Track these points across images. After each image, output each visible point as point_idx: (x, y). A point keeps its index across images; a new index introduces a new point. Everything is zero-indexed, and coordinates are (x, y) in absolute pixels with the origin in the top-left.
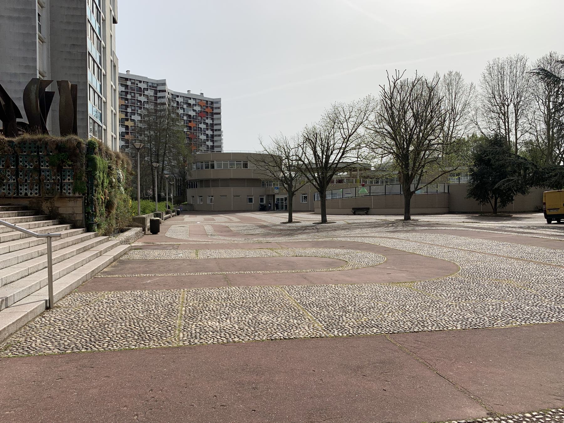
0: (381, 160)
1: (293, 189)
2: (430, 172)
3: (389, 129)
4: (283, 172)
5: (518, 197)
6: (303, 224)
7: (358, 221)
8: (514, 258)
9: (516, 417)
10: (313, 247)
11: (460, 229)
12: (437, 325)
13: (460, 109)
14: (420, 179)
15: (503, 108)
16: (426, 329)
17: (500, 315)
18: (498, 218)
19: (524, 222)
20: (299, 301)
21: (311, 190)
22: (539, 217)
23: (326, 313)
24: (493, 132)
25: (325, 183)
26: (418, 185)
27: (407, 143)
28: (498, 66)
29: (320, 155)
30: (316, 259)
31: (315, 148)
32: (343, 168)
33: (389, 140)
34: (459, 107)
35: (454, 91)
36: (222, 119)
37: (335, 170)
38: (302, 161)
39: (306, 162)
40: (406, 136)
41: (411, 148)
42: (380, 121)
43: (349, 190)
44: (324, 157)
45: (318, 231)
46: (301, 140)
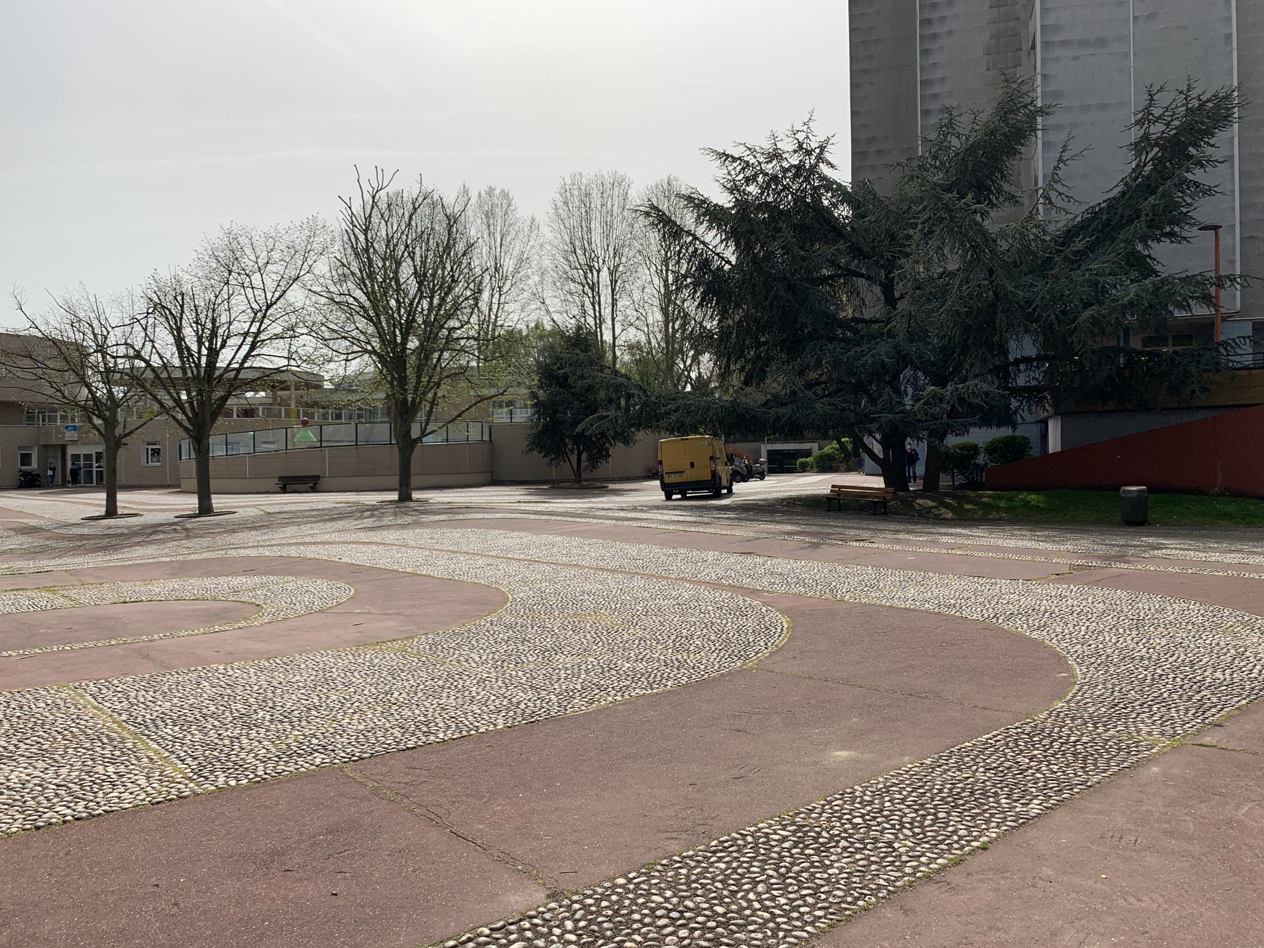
0: (346, 365)
1: (119, 431)
2: (451, 396)
3: (363, 299)
5: (617, 450)
6: (149, 518)
7: (292, 508)
9: (600, 890)
10: (173, 575)
12: (457, 727)
13: (511, 269)
14: (430, 412)
15: (590, 275)
16: (432, 738)
17: (578, 687)
18: (560, 491)
19: (628, 499)
20: (124, 717)
22: (652, 489)
23: (198, 736)
24: (573, 321)
25: (208, 416)
26: (427, 424)
29: (194, 347)
31: (179, 329)
32: (253, 381)
34: (509, 265)
37: (232, 385)
38: (143, 359)
39: (156, 361)
41: (413, 343)
43: (270, 435)
44: (204, 351)
45: (189, 534)
46: (141, 306)
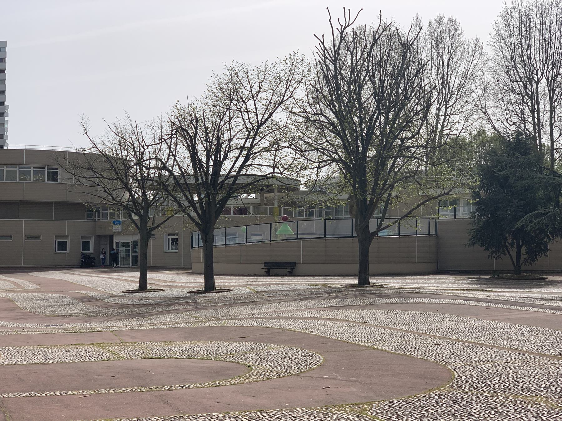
0: (319, 172)
1: (150, 225)
2: (404, 196)
3: (332, 116)
4: (130, 190)
6: (170, 293)
7: (275, 288)
8: (547, 356)
10: (186, 339)
11: (456, 302)
13: (456, 85)
14: (385, 210)
15: (529, 87)
21: (185, 227)
24: (513, 128)
26: (382, 220)
27: (362, 143)
28: (520, 11)
29: (204, 160)
30: (187, 362)
31: (194, 146)
32: (247, 185)
33: (331, 137)
34: (455, 81)
35: (446, 51)
36: (7, 60)
37: (231, 189)
39: (176, 171)
40: (362, 130)
41: (372, 153)
42: (317, 101)
44: (211, 163)
45: (197, 306)
46: (167, 129)
